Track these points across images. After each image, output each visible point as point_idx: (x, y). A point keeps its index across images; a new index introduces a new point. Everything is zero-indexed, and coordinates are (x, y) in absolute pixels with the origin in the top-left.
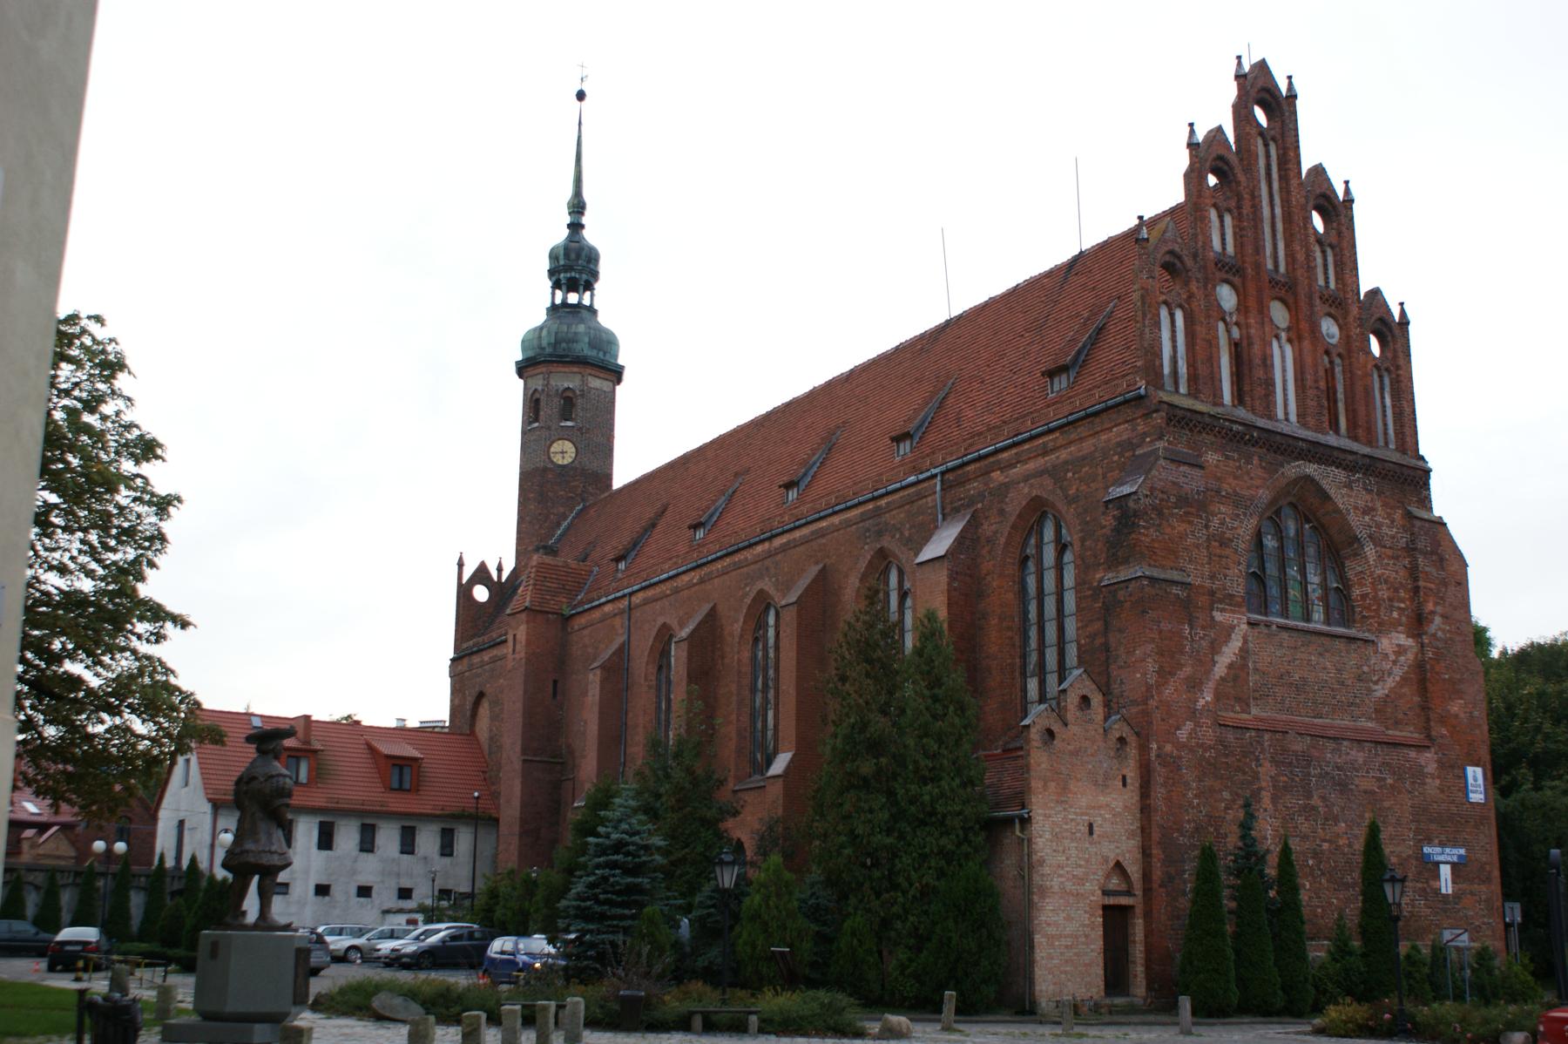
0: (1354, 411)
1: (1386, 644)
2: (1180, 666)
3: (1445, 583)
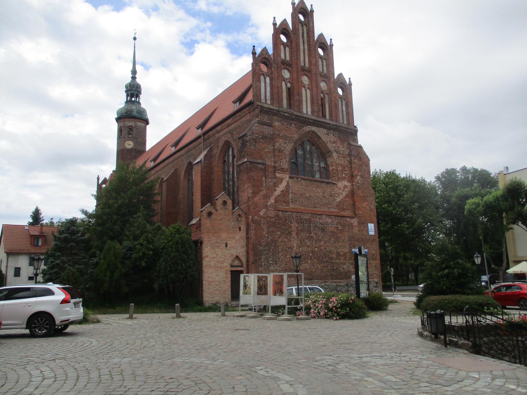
0: (332, 111)
1: (340, 184)
2: (261, 191)
3: (361, 165)
